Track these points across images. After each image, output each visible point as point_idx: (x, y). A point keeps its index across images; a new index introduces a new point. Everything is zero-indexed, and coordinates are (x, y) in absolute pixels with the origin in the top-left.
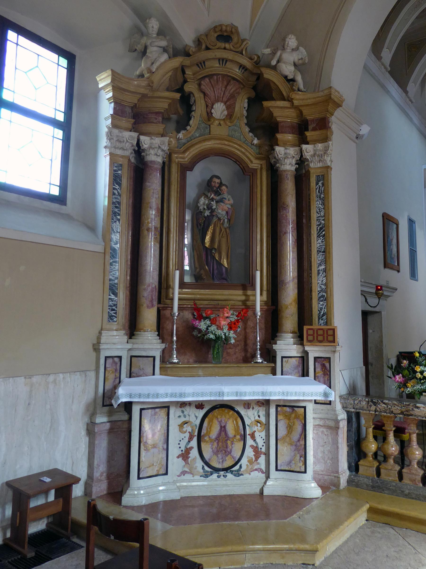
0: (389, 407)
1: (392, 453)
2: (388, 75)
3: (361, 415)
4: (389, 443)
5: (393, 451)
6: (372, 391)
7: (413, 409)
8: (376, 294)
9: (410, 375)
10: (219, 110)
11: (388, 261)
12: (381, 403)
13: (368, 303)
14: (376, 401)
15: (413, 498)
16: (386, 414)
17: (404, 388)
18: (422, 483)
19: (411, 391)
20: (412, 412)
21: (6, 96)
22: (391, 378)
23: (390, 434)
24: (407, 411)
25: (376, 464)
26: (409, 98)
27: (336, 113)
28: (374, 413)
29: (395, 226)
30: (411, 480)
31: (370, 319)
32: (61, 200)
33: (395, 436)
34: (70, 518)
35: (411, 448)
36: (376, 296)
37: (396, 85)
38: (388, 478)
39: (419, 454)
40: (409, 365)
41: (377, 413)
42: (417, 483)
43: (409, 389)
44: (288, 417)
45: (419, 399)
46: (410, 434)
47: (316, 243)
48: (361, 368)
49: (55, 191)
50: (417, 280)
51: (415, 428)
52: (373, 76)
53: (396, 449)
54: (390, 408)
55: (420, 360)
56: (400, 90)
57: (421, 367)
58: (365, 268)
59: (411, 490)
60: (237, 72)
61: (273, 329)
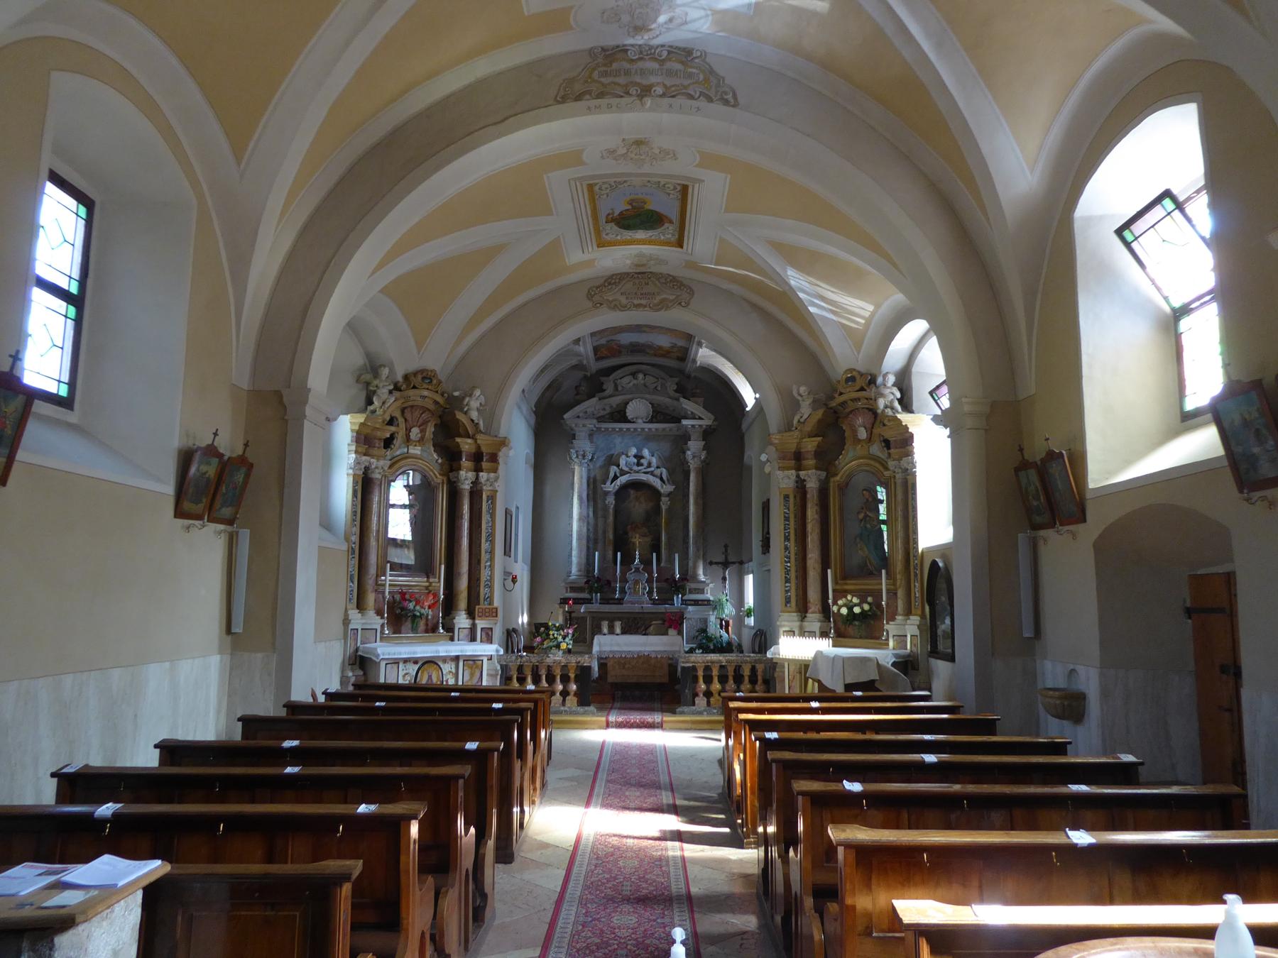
10: (415, 433)
21: (391, 502)
32: (65, 403)
34: (888, 669)
44: (471, 668)
47: (485, 546)
49: (64, 391)
60: (432, 407)
61: (449, 606)
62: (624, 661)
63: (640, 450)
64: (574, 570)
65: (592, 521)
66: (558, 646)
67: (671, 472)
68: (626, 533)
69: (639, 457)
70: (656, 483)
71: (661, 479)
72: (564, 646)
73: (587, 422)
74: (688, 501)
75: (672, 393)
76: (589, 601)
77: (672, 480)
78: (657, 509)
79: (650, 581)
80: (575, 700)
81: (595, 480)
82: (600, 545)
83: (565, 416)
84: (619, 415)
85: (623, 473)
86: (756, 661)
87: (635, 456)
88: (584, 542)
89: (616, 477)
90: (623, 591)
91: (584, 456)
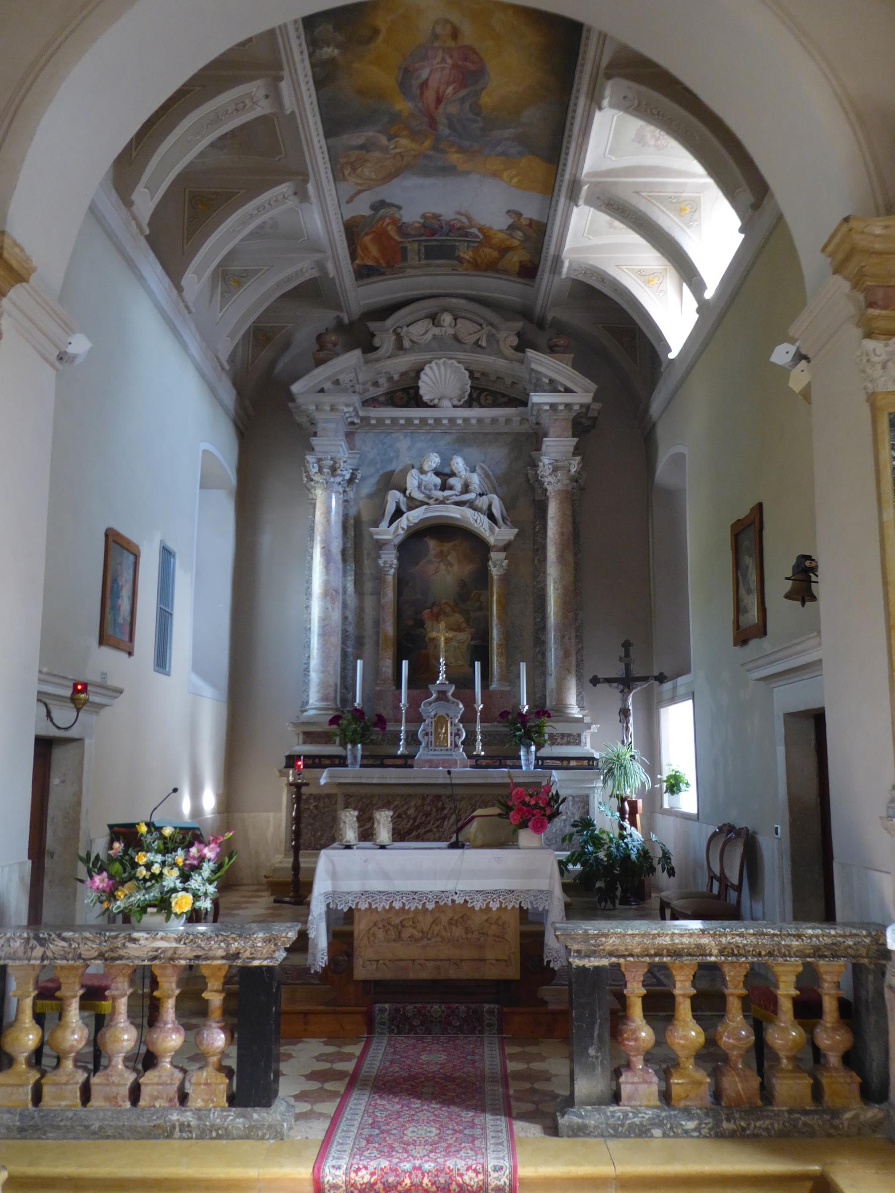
0: (74, 945)
1: (72, 1046)
2: (143, 243)
3: (10, 971)
4: (66, 1027)
5: (75, 1043)
6: (48, 913)
7: (124, 945)
8: (73, 700)
9: (125, 872)
11: (109, 631)
12: (56, 939)
13: (52, 721)
14: (46, 936)
15: (108, 1137)
16: (65, 962)
17: (110, 901)
18: (130, 1099)
19: (122, 906)
20: (122, 952)
22: (82, 881)
23: (70, 1005)
24: (112, 950)
25: (34, 1076)
26: (183, 301)
27: (12, 293)
28: (38, 962)
29: (132, 557)
30: (107, 1099)
31: (58, 755)
33: (82, 1008)
35: (113, 1029)
36: (72, 705)
37: (159, 267)
38: (57, 1103)
39: (128, 1040)
40: (125, 852)
41: (46, 962)
42: (120, 1103)
43: (118, 903)
45: (139, 922)
46: (114, 999)
48: (21, 864)
50: (168, 674)
51: (126, 985)
52: (110, 235)
53: (81, 1037)
54: (75, 948)
55: (149, 839)
56: (167, 280)
57: (149, 854)
58: (53, 642)
59: (106, 1120)
62: (402, 920)
63: (446, 460)
64: (314, 697)
65: (352, 602)
66: (164, 904)
67: (509, 504)
68: (420, 624)
69: (445, 475)
70: (480, 524)
71: (491, 516)
72: (182, 903)
73: (340, 400)
74: (544, 559)
75: (510, 352)
76: (340, 761)
77: (510, 518)
78: (482, 577)
79: (468, 719)
80: (221, 1084)
81: (358, 521)
82: (369, 647)
83: (295, 388)
84: (407, 394)
85: (413, 504)
86: (818, 952)
87: (437, 473)
88: (336, 640)
89: (398, 513)
90: (413, 740)
91: (334, 470)
